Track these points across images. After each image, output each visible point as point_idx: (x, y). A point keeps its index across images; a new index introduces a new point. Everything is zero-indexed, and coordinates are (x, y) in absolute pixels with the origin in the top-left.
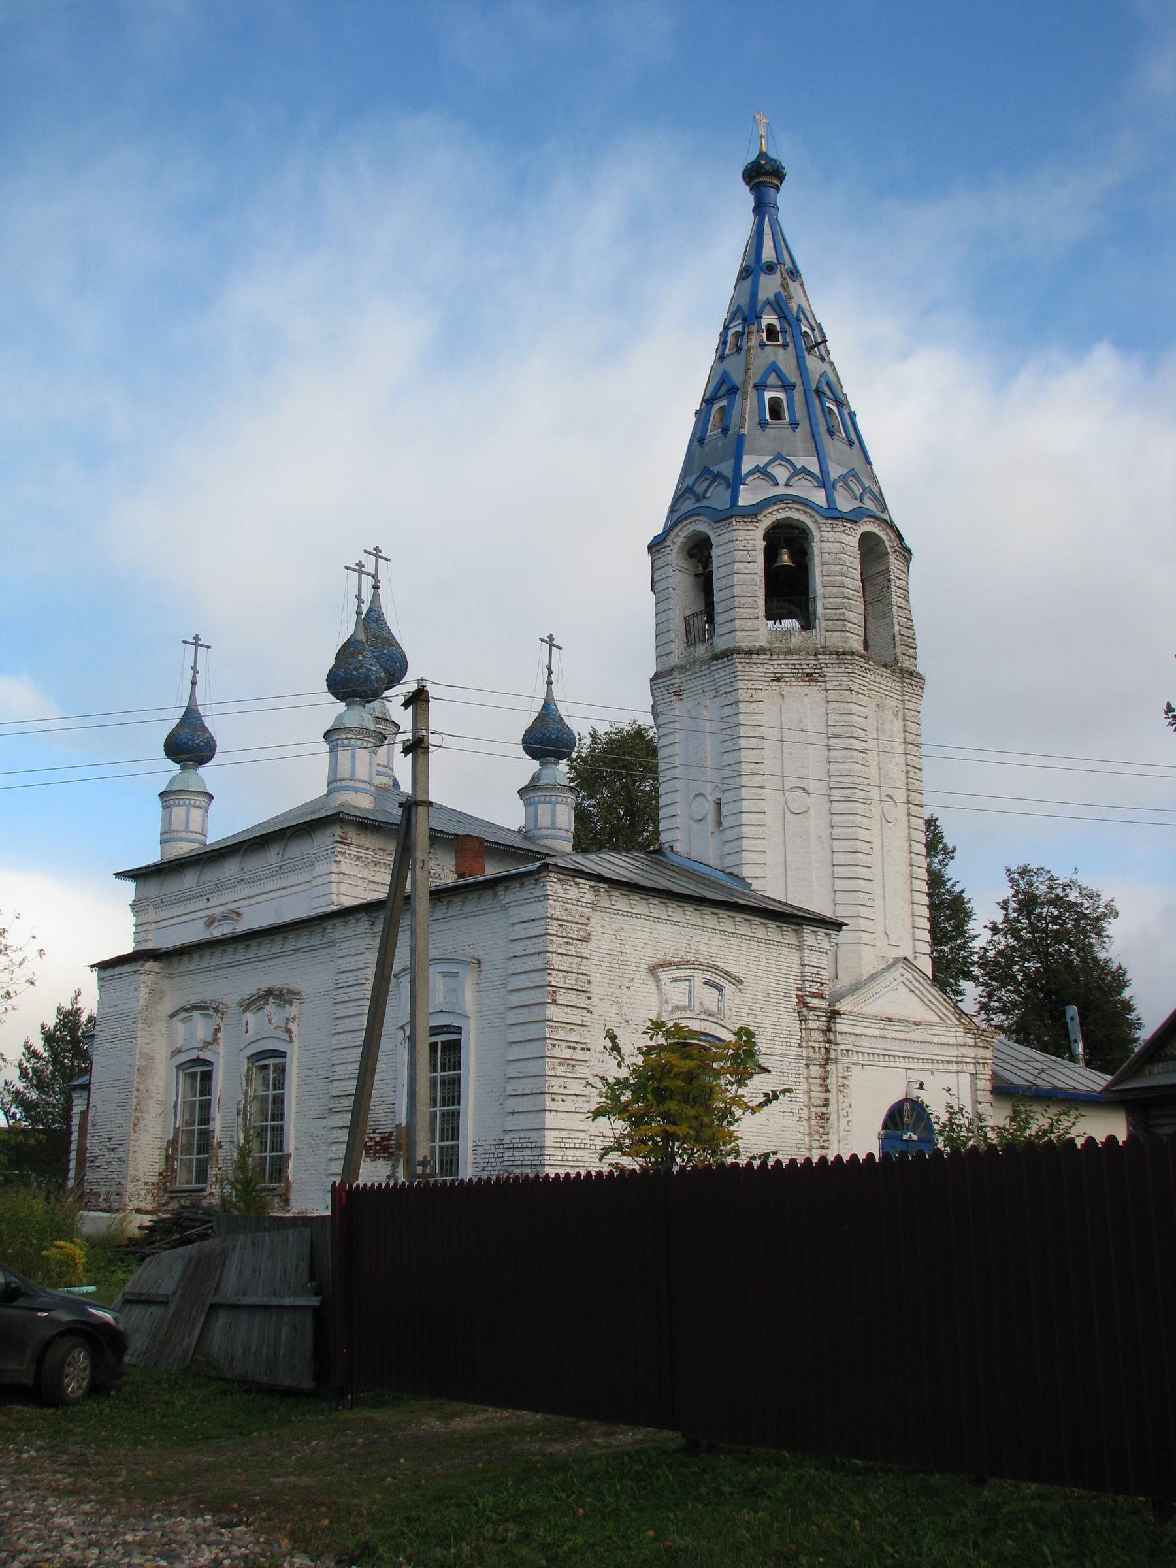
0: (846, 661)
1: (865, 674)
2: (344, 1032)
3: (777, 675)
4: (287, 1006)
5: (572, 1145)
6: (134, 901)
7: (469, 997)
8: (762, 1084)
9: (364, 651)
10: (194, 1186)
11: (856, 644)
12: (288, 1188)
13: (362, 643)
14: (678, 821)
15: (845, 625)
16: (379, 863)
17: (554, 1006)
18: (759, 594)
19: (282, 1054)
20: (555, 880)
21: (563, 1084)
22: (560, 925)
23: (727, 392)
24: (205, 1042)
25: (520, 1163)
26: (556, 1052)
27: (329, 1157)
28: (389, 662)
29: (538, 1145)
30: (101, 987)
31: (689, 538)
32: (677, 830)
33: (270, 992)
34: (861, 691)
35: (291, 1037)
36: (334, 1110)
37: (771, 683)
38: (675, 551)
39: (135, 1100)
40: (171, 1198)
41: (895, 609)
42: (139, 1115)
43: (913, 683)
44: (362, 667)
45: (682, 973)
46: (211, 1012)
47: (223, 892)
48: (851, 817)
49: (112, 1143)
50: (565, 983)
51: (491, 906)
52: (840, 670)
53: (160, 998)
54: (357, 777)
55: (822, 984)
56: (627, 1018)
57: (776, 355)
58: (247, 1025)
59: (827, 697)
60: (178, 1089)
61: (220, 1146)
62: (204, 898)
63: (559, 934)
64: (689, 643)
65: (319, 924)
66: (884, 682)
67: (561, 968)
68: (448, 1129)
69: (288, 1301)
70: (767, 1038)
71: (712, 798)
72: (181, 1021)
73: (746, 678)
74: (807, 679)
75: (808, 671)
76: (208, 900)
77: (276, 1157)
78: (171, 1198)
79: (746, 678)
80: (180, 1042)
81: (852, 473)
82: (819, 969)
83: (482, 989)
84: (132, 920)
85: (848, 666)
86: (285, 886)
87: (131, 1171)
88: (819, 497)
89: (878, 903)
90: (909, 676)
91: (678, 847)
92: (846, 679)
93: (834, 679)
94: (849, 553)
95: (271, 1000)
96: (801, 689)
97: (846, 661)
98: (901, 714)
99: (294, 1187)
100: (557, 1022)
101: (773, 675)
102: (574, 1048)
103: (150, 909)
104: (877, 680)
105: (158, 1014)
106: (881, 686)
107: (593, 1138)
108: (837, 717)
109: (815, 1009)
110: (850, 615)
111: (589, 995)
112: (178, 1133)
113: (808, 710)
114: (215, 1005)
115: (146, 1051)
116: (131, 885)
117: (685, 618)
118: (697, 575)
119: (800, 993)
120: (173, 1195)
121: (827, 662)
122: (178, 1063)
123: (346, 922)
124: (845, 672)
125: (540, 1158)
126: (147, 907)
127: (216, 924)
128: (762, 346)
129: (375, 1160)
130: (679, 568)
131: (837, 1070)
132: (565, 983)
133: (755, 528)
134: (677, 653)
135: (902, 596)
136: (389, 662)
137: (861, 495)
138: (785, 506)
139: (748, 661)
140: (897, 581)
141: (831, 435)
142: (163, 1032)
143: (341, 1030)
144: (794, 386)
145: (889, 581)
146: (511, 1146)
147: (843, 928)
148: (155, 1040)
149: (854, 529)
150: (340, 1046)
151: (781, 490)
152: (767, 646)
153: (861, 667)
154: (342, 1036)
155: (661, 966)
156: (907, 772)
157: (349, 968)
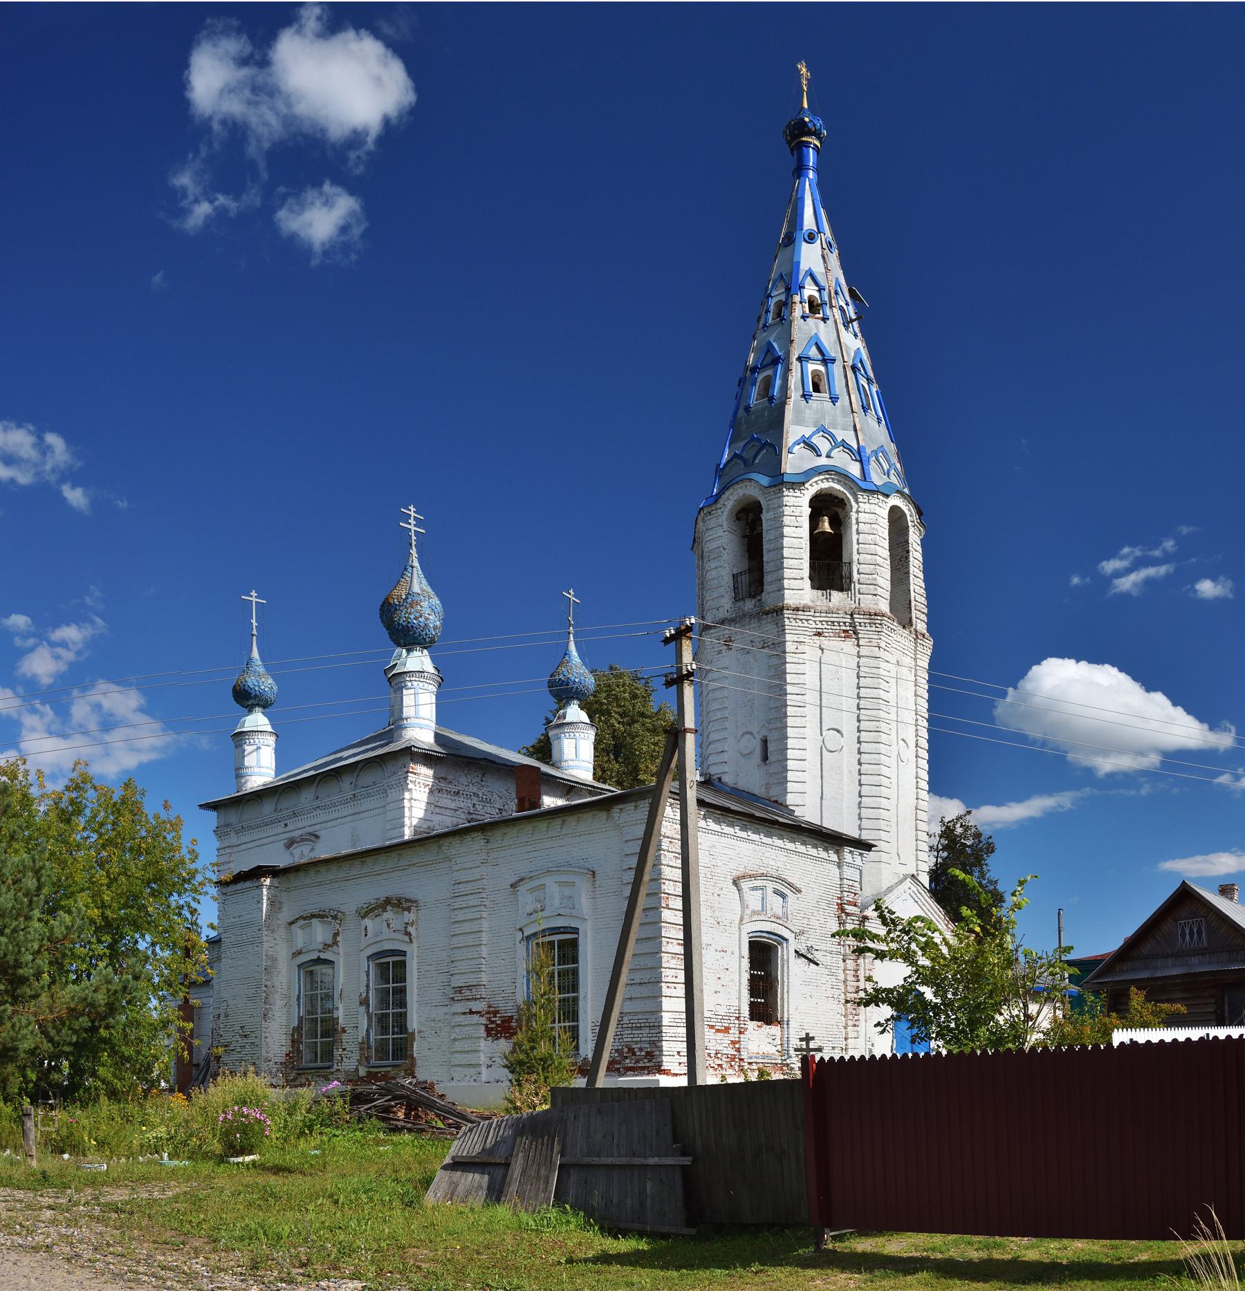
0: (877, 621)
2: (462, 934)
4: (406, 913)
6: (217, 828)
7: (585, 903)
10: (319, 1064)
11: (884, 606)
12: (413, 1064)
14: (725, 757)
16: (442, 790)
19: (403, 953)
22: (670, 842)
23: (772, 362)
24: (325, 945)
25: (639, 1039)
27: (452, 1037)
29: (656, 1024)
32: (725, 765)
33: (388, 901)
35: (410, 939)
36: (456, 998)
37: (813, 638)
38: (726, 513)
39: (264, 995)
40: (299, 1074)
41: (912, 577)
42: (268, 1007)
44: (421, 616)
45: (758, 883)
46: (330, 919)
47: (300, 818)
48: (876, 756)
50: (675, 890)
51: (604, 826)
53: (280, 908)
55: (855, 894)
56: (719, 920)
57: (817, 327)
58: (366, 929)
60: (299, 984)
61: (344, 1031)
62: (282, 824)
63: (670, 850)
64: (737, 599)
66: (903, 642)
67: (672, 878)
68: (569, 1012)
69: (652, 1161)
71: (759, 737)
72: (299, 927)
73: (793, 632)
74: (843, 635)
75: (844, 628)
76: (286, 825)
77: (397, 1038)
78: (299, 1074)
79: (793, 632)
80: (300, 944)
81: (882, 449)
83: (597, 896)
86: (358, 811)
87: (264, 1053)
88: (854, 470)
89: (893, 829)
91: (725, 779)
92: (876, 637)
93: (866, 636)
95: (389, 908)
97: (877, 621)
99: (419, 1063)
103: (232, 834)
104: (898, 640)
109: (852, 915)
110: (881, 581)
114: (332, 913)
115: (271, 953)
116: (213, 815)
117: (733, 575)
118: (744, 537)
119: (839, 901)
120: (301, 1072)
121: (862, 621)
122: (299, 963)
125: (658, 1035)
127: (295, 845)
128: (804, 317)
129: (497, 1039)
131: (864, 963)
132: (675, 890)
133: (801, 495)
134: (728, 607)
137: (888, 471)
139: (795, 617)
140: (914, 552)
141: (864, 411)
143: (460, 932)
145: (908, 552)
146: (630, 1025)
147: (873, 849)
148: (277, 944)
150: (459, 945)
151: (823, 461)
152: (810, 604)
154: (461, 938)
155: (744, 877)
157: (465, 880)
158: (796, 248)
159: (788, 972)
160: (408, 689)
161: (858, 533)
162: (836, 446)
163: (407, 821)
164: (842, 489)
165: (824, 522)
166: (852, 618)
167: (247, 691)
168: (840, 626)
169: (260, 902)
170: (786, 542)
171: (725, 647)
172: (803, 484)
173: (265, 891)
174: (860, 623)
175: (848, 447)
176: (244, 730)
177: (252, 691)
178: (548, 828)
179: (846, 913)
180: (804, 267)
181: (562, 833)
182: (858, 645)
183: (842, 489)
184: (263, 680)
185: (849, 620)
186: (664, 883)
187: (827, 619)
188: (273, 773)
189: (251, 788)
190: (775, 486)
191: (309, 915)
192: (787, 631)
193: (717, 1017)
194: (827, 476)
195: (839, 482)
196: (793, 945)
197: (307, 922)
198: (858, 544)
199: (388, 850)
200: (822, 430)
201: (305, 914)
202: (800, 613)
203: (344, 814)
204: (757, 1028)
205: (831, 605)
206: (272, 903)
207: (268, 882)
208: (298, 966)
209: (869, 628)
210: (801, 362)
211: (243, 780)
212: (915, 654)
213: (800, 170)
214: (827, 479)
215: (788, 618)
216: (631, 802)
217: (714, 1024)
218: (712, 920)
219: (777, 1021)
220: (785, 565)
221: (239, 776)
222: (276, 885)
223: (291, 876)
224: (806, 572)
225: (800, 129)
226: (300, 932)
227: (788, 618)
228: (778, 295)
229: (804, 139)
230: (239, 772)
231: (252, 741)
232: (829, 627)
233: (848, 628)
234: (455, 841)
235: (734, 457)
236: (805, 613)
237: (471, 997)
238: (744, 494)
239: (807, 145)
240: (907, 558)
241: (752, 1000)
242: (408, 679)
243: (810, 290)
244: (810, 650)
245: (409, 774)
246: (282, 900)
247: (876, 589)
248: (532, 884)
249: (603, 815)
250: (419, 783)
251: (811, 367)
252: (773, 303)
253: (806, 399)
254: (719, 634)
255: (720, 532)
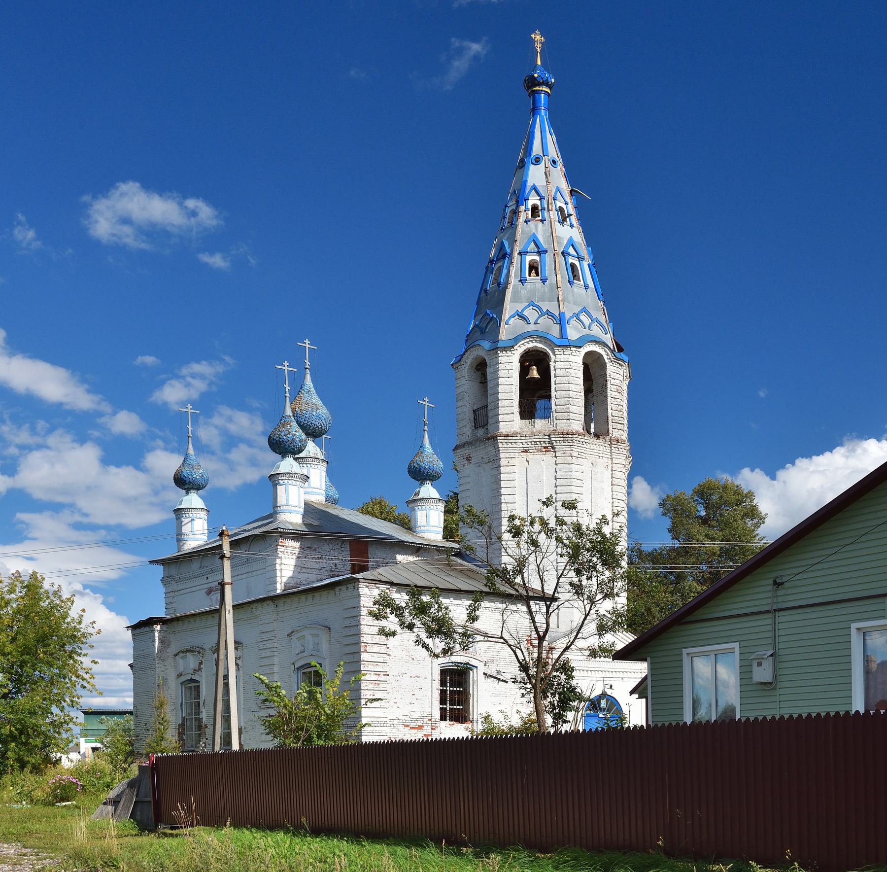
0: (568, 439)
1: (582, 446)
3: (525, 449)
5: (379, 725)
8: (502, 689)
9: (291, 422)
13: (290, 417)
15: (569, 415)
17: (366, 653)
18: (514, 397)
20: (363, 586)
21: (372, 694)
23: (502, 256)
24: (195, 670)
26: (367, 677)
28: (317, 420)
30: (134, 639)
31: (475, 359)
34: (579, 456)
37: (522, 454)
43: (619, 447)
44: (289, 434)
46: (196, 653)
47: (216, 573)
49: (147, 726)
50: (372, 640)
51: (334, 599)
52: (565, 444)
54: (290, 503)
56: (413, 657)
57: (536, 227)
59: (556, 461)
60: (182, 696)
62: (205, 577)
65: (249, 606)
70: (506, 664)
72: (181, 658)
73: (505, 451)
74: (544, 450)
75: (545, 445)
76: (207, 578)
79: (505, 451)
80: (181, 669)
82: (542, 624)
84: (163, 590)
85: (570, 441)
90: (616, 443)
92: (569, 449)
93: (561, 449)
94: (574, 368)
96: (539, 456)
97: (568, 439)
98: (610, 467)
100: (368, 661)
101: (523, 449)
102: (379, 675)
104: (592, 448)
105: (168, 654)
106: (595, 451)
107: (392, 721)
108: (563, 473)
110: (573, 408)
111: (388, 646)
112: (184, 720)
113: (544, 470)
114: (198, 649)
116: (160, 568)
117: (474, 411)
121: (557, 439)
122: (181, 681)
123: (262, 605)
124: (568, 446)
126: (171, 582)
127: (213, 593)
130: (470, 379)
133: (512, 355)
134: (468, 433)
135: (616, 390)
136: (317, 420)
138: (532, 339)
139: (506, 441)
142: (172, 664)
143: (263, 664)
144: (547, 251)
145: (606, 381)
146: (346, 725)
148: (167, 669)
149: (579, 351)
151: (532, 327)
152: (519, 431)
153: (579, 441)
156: (613, 503)
158: (525, 171)
159: (477, 688)
160: (280, 485)
161: (555, 377)
162: (542, 315)
163: (278, 579)
164: (543, 347)
165: (533, 370)
166: (550, 438)
167: (183, 479)
168: (541, 444)
169: (154, 641)
170: (500, 389)
171: (467, 462)
172: (513, 347)
173: (157, 634)
174: (556, 441)
175: (551, 314)
176: (181, 507)
177: (187, 479)
178: (306, 599)
179: (533, 646)
180: (530, 184)
181: (314, 602)
182: (556, 456)
183: (543, 347)
184: (195, 470)
185: (548, 440)
186: (363, 637)
187: (531, 440)
188: (206, 538)
189: (187, 550)
190: (493, 350)
191: (185, 650)
192: (501, 451)
193: (411, 719)
194: (530, 339)
195: (541, 342)
196: (482, 669)
197: (184, 654)
198: (556, 384)
199: (201, 615)
200: (532, 304)
201: (183, 649)
202: (510, 438)
203: (243, 572)
204: (449, 726)
205: (535, 430)
206: (162, 641)
207: (158, 627)
208: (181, 683)
209: (563, 444)
210: (521, 255)
211: (181, 544)
212: (611, 455)
213: (535, 110)
214: (531, 341)
215: (501, 442)
216: (344, 585)
217: (409, 724)
218: (408, 658)
219: (470, 720)
220: (500, 405)
221: (179, 540)
222: (165, 630)
223: (175, 623)
224: (516, 409)
225: (532, 83)
226: (181, 661)
227: (501, 442)
228: (512, 205)
229: (535, 89)
230: (179, 538)
231: (187, 515)
232: (533, 446)
233: (548, 445)
234: (259, 605)
235: (475, 326)
236: (513, 438)
237: (269, 706)
238: (477, 355)
239: (539, 92)
240: (606, 385)
241: (441, 706)
242: (280, 478)
243: (533, 200)
244: (519, 460)
245: (278, 547)
246: (171, 640)
247: (569, 415)
248: (298, 635)
249: (332, 592)
250: (287, 552)
251: (528, 258)
252: (509, 211)
253: (522, 283)
254: (462, 453)
255: (463, 381)
